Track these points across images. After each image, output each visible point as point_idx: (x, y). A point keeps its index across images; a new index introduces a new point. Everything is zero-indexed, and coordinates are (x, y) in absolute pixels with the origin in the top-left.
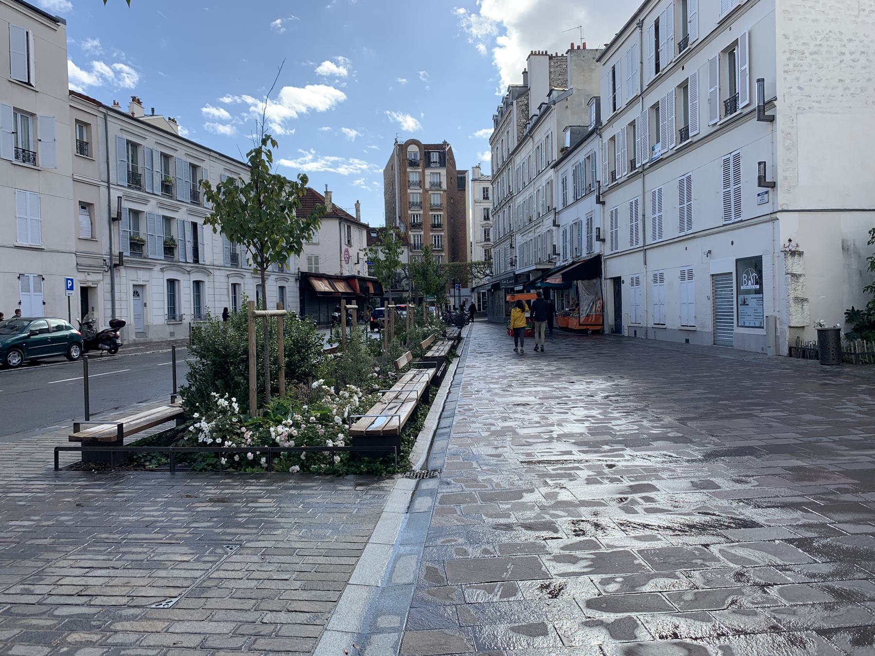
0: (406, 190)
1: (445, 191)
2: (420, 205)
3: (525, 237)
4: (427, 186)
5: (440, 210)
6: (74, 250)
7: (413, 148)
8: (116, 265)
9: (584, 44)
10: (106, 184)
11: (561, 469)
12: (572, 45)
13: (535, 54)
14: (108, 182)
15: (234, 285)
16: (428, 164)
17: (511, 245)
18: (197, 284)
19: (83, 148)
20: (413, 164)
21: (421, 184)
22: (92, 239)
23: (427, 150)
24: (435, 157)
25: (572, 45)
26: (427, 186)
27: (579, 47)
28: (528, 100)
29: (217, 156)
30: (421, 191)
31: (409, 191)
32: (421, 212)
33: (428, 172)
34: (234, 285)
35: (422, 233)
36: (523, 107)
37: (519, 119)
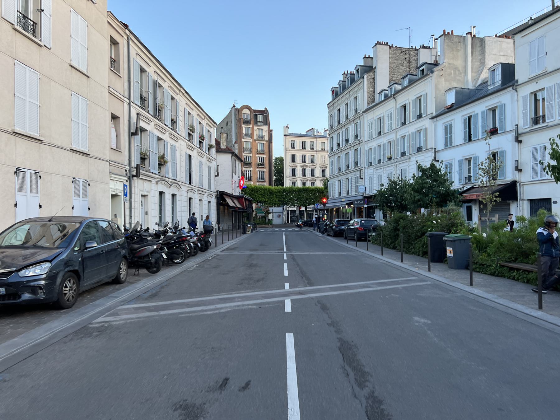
0: (241, 140)
1: (266, 141)
2: (250, 150)
3: (378, 171)
4: (255, 137)
5: (263, 154)
6: (108, 159)
7: (246, 111)
8: (133, 176)
9: (452, 31)
10: (128, 101)
11: (148, 309)
12: (444, 31)
13: (380, 44)
14: (129, 99)
15: (190, 199)
16: (256, 122)
17: (360, 176)
18: (173, 195)
19: (114, 63)
20: (247, 122)
21: (250, 136)
22: (117, 150)
23: (256, 113)
24: (260, 118)
25: (444, 31)
26: (255, 137)
27: (448, 33)
28: (374, 75)
29: (184, 92)
30: (251, 141)
31: (243, 140)
32: (251, 155)
33: (256, 128)
34: (190, 199)
35: (252, 169)
36: (371, 80)
37: (368, 88)
